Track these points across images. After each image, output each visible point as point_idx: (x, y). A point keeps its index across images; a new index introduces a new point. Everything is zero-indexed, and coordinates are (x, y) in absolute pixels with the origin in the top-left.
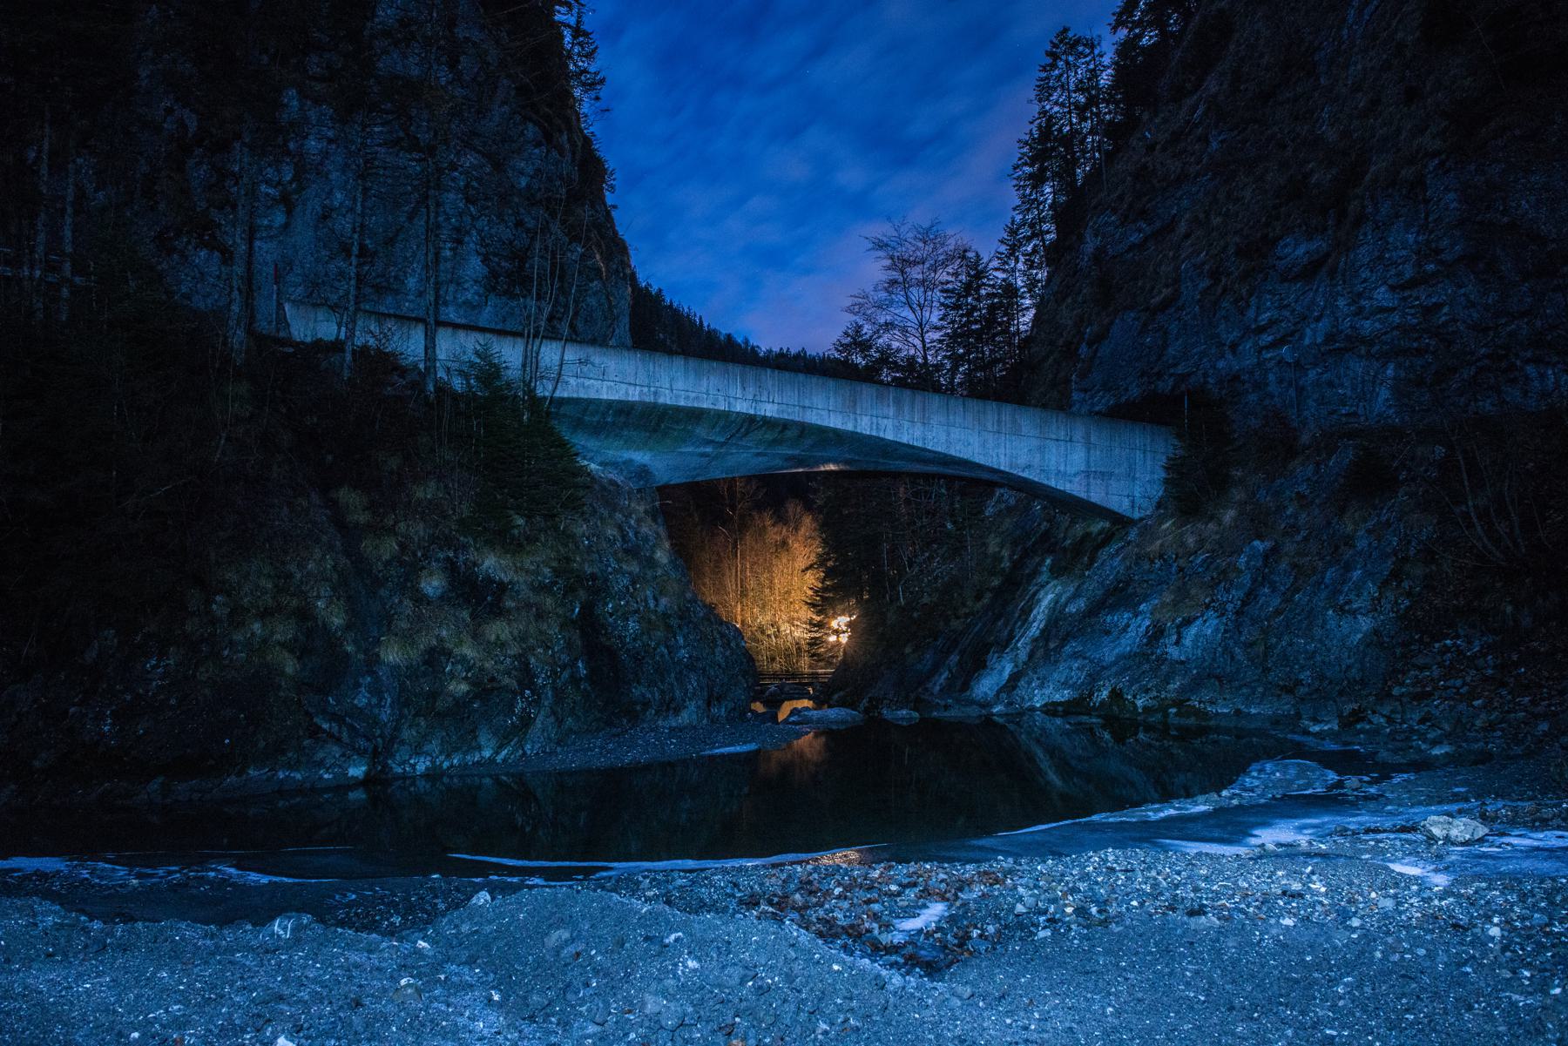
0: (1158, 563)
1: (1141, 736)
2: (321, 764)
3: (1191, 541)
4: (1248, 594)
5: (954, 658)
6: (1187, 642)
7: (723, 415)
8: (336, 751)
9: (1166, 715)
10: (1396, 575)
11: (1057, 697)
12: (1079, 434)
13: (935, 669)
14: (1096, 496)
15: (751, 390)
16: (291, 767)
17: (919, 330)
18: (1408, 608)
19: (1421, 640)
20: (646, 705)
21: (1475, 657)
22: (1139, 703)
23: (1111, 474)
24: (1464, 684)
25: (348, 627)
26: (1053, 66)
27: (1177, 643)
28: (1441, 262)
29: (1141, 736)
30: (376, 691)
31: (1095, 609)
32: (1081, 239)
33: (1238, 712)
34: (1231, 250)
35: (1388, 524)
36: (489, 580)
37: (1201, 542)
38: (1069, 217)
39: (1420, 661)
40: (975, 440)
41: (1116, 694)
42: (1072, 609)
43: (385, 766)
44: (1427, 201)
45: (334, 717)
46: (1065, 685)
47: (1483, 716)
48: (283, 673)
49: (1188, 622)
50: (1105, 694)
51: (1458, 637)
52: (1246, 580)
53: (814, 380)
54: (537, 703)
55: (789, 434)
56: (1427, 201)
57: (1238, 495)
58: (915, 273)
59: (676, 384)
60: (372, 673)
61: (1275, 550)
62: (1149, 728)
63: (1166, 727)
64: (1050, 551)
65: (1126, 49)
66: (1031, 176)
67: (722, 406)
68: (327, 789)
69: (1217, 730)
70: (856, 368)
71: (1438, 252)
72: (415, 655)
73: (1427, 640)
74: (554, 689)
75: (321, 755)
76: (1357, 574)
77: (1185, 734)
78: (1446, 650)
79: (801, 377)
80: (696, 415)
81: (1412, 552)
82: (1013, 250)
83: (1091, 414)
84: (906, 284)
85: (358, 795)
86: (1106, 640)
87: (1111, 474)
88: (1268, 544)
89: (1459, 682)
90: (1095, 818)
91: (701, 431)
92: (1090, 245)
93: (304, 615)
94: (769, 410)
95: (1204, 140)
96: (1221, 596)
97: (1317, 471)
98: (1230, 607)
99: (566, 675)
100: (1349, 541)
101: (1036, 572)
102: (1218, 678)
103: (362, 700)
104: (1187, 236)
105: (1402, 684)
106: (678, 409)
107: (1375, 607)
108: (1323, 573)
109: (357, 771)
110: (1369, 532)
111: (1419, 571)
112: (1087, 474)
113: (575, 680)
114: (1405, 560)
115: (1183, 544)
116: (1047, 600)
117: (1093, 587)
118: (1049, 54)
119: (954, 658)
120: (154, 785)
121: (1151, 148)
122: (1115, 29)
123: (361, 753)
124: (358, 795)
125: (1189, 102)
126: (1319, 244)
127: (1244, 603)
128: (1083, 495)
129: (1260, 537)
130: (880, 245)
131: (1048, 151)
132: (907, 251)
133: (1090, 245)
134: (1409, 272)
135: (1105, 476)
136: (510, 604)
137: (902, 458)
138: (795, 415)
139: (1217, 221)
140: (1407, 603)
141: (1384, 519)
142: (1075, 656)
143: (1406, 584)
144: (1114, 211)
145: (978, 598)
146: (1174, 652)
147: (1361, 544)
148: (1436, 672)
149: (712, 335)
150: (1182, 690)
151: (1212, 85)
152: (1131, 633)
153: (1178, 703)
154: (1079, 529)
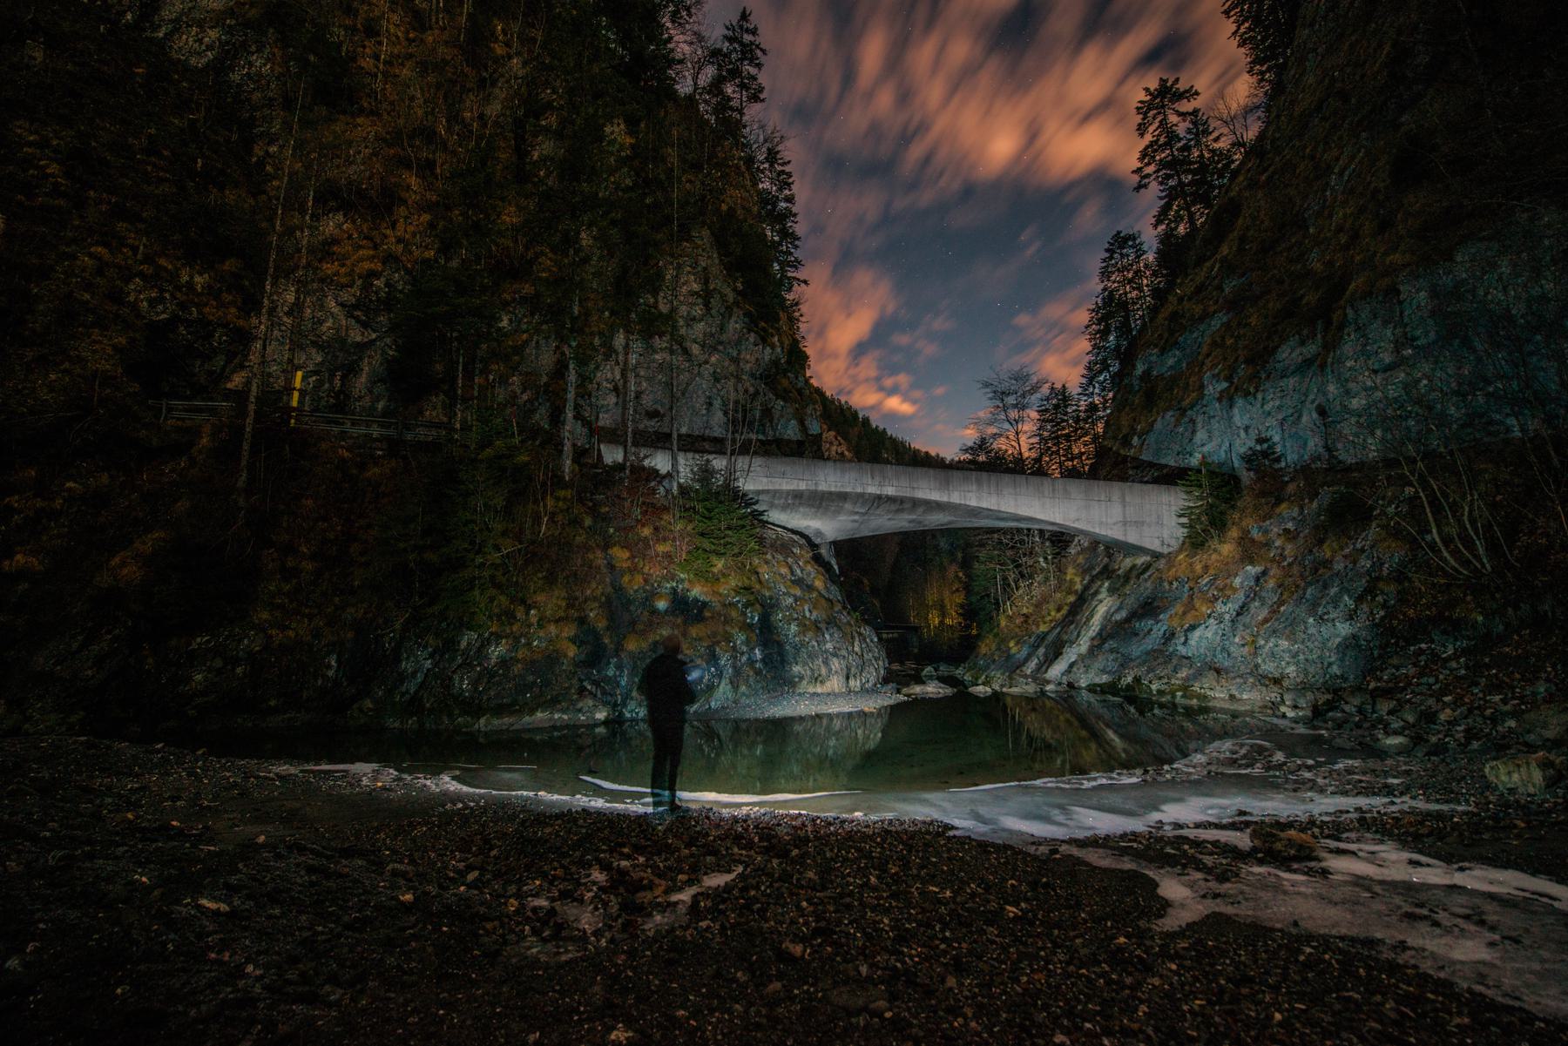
0: (1175, 584)
1: (1156, 711)
2: (580, 710)
3: (1198, 568)
4: (1242, 608)
5: (1042, 651)
6: (1192, 642)
7: (862, 495)
8: (591, 703)
9: (1174, 697)
10: (1370, 591)
11: (1097, 680)
12: (1116, 496)
13: (1027, 660)
14: (1132, 538)
15: (877, 479)
16: (563, 711)
17: (1024, 439)
18: (1382, 618)
19: (1396, 644)
20: (801, 678)
21: (1448, 659)
22: (1154, 687)
23: (1143, 523)
24: (1437, 681)
25: (608, 629)
26: (1111, 258)
27: (1185, 643)
28: (1414, 348)
29: (1156, 711)
30: (619, 667)
31: (1133, 616)
32: (1134, 366)
33: (1232, 697)
34: (1241, 359)
35: (1363, 550)
36: (696, 600)
37: (1206, 568)
38: (1127, 357)
39: (1395, 661)
40: (831, 478)
41: (1137, 680)
42: (1118, 617)
43: (621, 713)
44: (1400, 303)
45: (596, 683)
46: (1104, 671)
47: (1448, 711)
48: (565, 656)
49: (1193, 628)
50: (1129, 679)
51: (1432, 641)
52: (1241, 596)
53: (919, 469)
54: (720, 676)
55: (906, 506)
56: (1400, 303)
57: (1234, 533)
58: (1011, 400)
59: (871, 483)
60: (617, 656)
61: (1264, 573)
62: (1161, 706)
63: (1175, 705)
64: (1108, 578)
65: (1167, 239)
66: (1098, 331)
67: (859, 490)
68: (583, 726)
69: (1214, 710)
70: (986, 463)
71: (1414, 339)
72: (644, 645)
73: (1402, 643)
74: (734, 667)
75: (580, 705)
76: (1333, 591)
77: (1190, 713)
78: (1422, 652)
79: (910, 469)
80: (843, 497)
81: (1385, 572)
82: (1091, 381)
83: (1072, 474)
84: (1005, 408)
85: (601, 730)
86: (1135, 639)
87: (1143, 523)
88: (1259, 569)
89: (1432, 680)
90: (1038, 782)
91: (848, 506)
92: (1140, 368)
93: (582, 621)
94: (890, 491)
95: (1220, 288)
96: (1220, 607)
97: (1301, 513)
98: (1227, 617)
99: (744, 659)
100: (1327, 564)
101: (1097, 592)
102: (1218, 671)
103: (610, 673)
104: (1208, 355)
105: (1379, 679)
106: (831, 493)
107: (1351, 616)
108: (1305, 590)
109: (601, 715)
110: (1345, 557)
111: (1392, 588)
112: (1125, 523)
113: (751, 662)
114: (1378, 579)
115: (1193, 571)
116: (1101, 610)
117: (1131, 602)
118: (1107, 250)
119: (1042, 651)
120: (482, 721)
121: (1181, 299)
122: (1155, 226)
123: (605, 704)
124: (601, 730)
125: (1208, 264)
126: (1311, 349)
127: (1238, 614)
128: (1121, 538)
129: (1252, 563)
130: (987, 385)
131: (1110, 312)
132: (1004, 387)
133: (1140, 368)
134: (1387, 358)
135: (1139, 524)
136: (707, 614)
137: (987, 517)
138: (907, 493)
139: (1229, 342)
140: (1382, 613)
141: (1359, 546)
142: (1111, 651)
143: (1380, 599)
144: (1156, 346)
145: (1059, 610)
146: (1182, 650)
147: (1339, 566)
148: (1412, 671)
149: (916, 452)
150: (1187, 679)
151: (1225, 250)
152: (1154, 634)
153: (1185, 688)
154: (1128, 562)
